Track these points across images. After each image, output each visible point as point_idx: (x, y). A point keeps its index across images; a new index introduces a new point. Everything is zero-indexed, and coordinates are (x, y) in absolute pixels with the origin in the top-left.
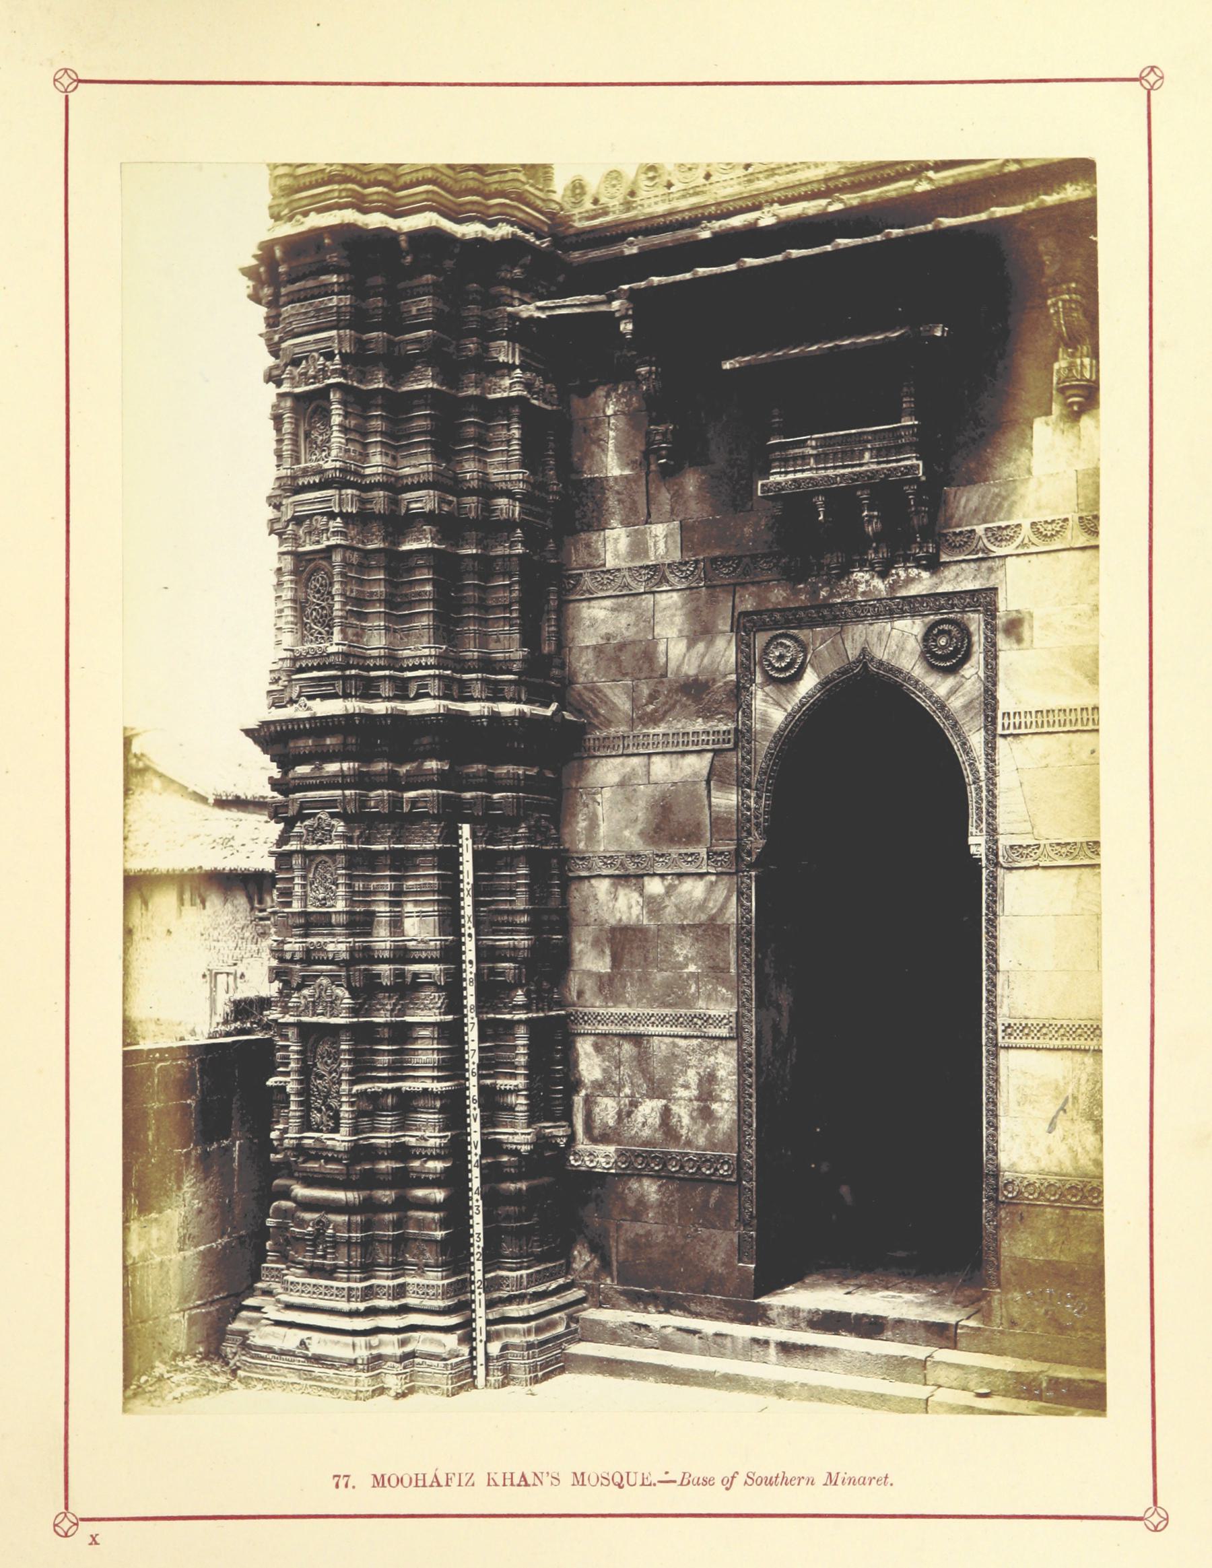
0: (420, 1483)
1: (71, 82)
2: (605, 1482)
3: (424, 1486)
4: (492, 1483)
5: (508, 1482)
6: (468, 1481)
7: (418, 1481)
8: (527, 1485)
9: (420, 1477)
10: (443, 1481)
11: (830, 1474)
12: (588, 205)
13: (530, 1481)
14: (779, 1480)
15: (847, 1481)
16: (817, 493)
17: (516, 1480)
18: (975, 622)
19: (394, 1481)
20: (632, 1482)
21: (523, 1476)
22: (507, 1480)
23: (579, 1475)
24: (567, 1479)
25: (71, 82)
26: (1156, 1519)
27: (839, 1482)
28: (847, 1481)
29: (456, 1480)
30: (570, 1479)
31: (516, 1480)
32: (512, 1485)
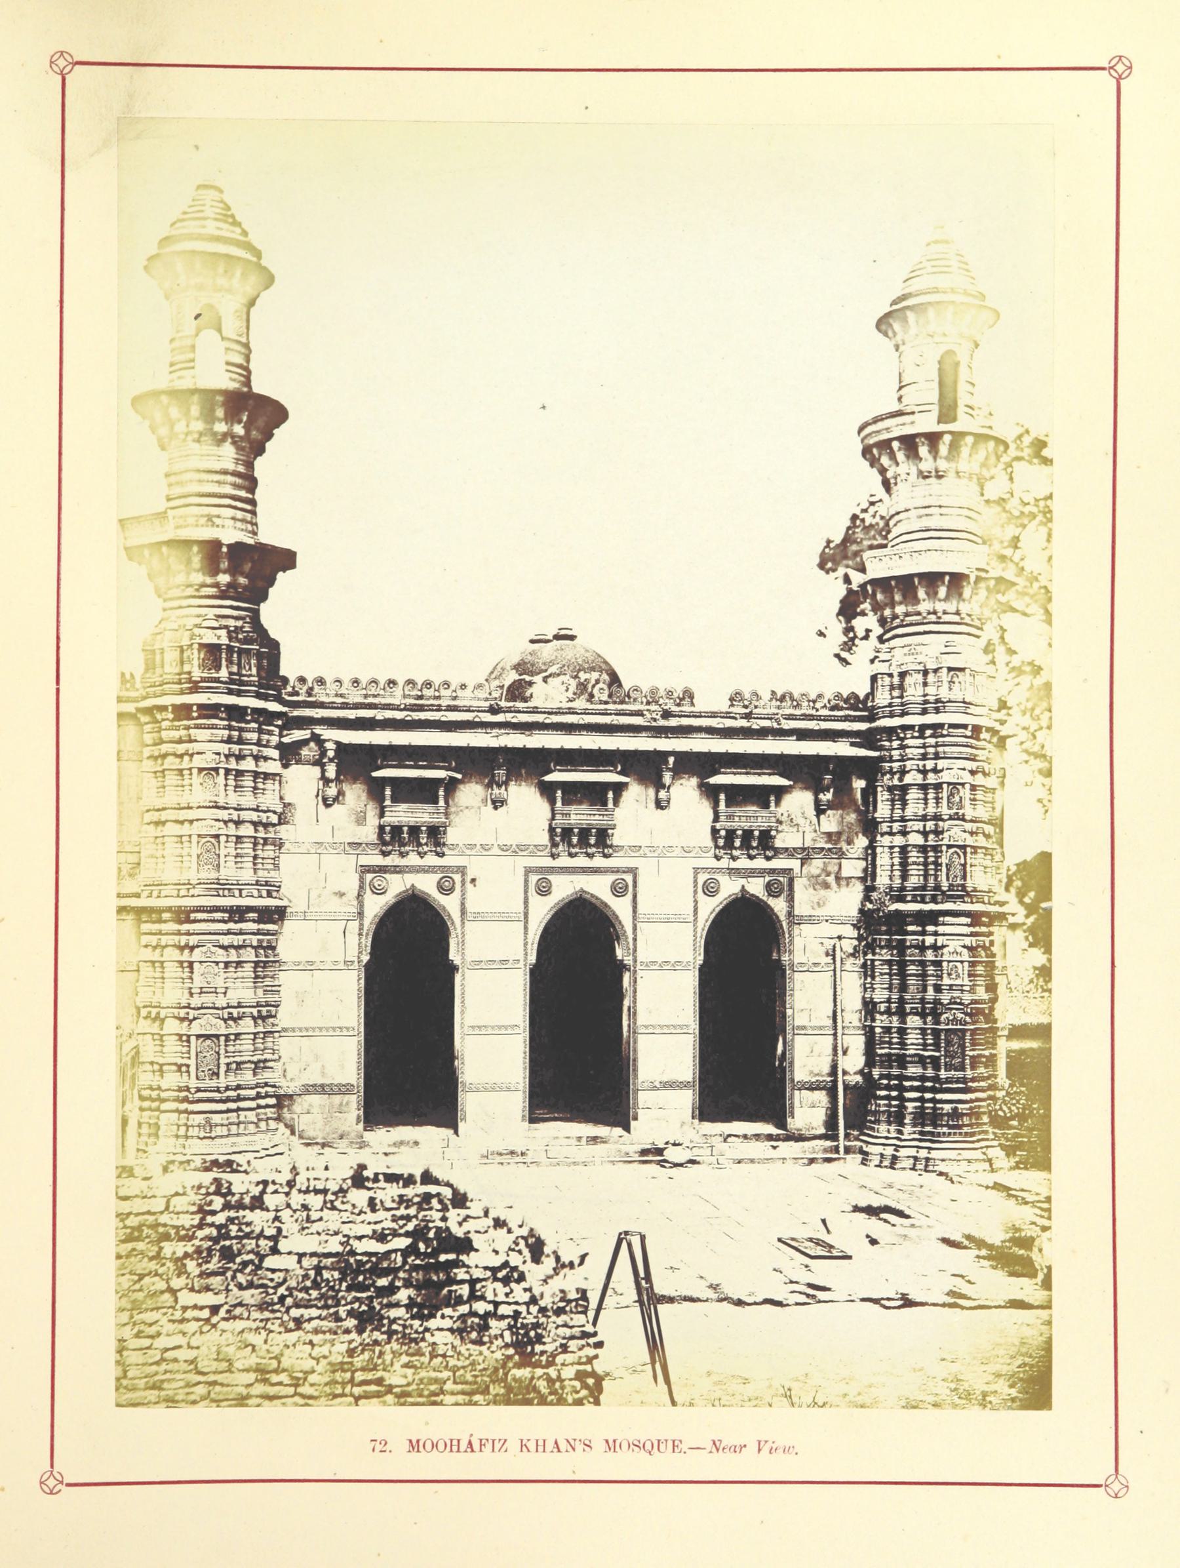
0: (455, 1448)
2: (636, 1449)
9: (455, 1443)
10: (476, 1446)
11: (411, 1441)
12: (289, 689)
16: (863, 905)
18: (457, 878)
19: (441, 1446)
21: (556, 1443)
23: (611, 1443)
26: (1116, 1486)
29: (489, 1446)
32: (458, 1451)
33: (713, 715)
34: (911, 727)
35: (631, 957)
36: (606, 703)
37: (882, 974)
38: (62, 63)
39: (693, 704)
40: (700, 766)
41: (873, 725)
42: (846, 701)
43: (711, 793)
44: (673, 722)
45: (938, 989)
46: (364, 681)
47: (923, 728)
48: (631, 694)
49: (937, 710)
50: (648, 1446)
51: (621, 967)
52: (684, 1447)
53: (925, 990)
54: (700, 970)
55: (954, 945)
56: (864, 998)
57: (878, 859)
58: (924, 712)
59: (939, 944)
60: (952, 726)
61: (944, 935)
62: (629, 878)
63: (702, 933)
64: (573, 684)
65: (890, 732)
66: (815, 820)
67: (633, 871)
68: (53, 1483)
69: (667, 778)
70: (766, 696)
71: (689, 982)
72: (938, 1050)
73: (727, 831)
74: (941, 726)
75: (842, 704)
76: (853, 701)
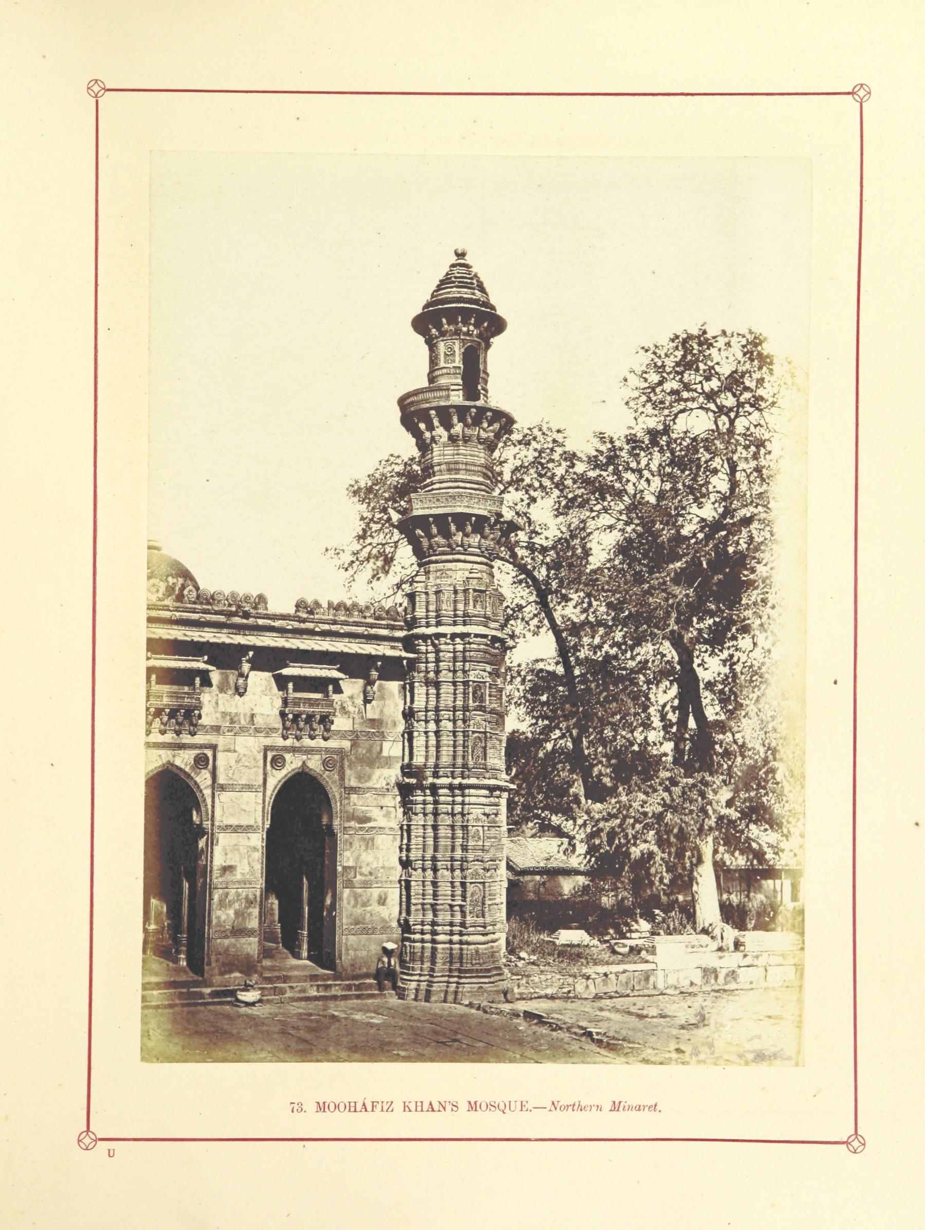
1: (98, 90)
2: (493, 1108)
3: (355, 1111)
4: (407, 1109)
5: (419, 1109)
6: (389, 1107)
7: (351, 1107)
8: (433, 1110)
9: (352, 1104)
10: (369, 1107)
13: (436, 1108)
14: (576, 1107)
15: (627, 1108)
17: (359, 1107)
19: (342, 1107)
20: (512, 1109)
21: (431, 1104)
22: (419, 1107)
23: (473, 1103)
24: (464, 1106)
25: (98, 90)
27: (621, 1109)
28: (627, 1108)
29: (379, 1107)
30: (467, 1106)
31: (359, 1107)
32: (422, 1110)
33: (284, 617)
34: (444, 635)
35: (209, 822)
36: (194, 603)
37: (417, 837)
38: (96, 88)
39: (266, 609)
40: (269, 660)
41: (411, 632)
42: (388, 612)
43: (281, 682)
44: (251, 621)
45: (465, 849)
46: (729, 333)
47: (454, 636)
48: (216, 597)
49: (465, 624)
50: (502, 1106)
51: (200, 832)
52: (529, 1106)
53: (453, 850)
54: (268, 833)
55: (477, 812)
56: (400, 859)
57: (415, 741)
58: (455, 624)
59: (466, 812)
60: (476, 636)
61: (469, 804)
62: (209, 753)
63: (270, 800)
64: (163, 587)
65: (425, 637)
66: (363, 707)
67: (214, 747)
68: (88, 1138)
69: (246, 667)
70: (325, 605)
71: (257, 840)
72: (464, 901)
73: (294, 715)
74: (468, 635)
75: (384, 615)
76: (391, 614)
